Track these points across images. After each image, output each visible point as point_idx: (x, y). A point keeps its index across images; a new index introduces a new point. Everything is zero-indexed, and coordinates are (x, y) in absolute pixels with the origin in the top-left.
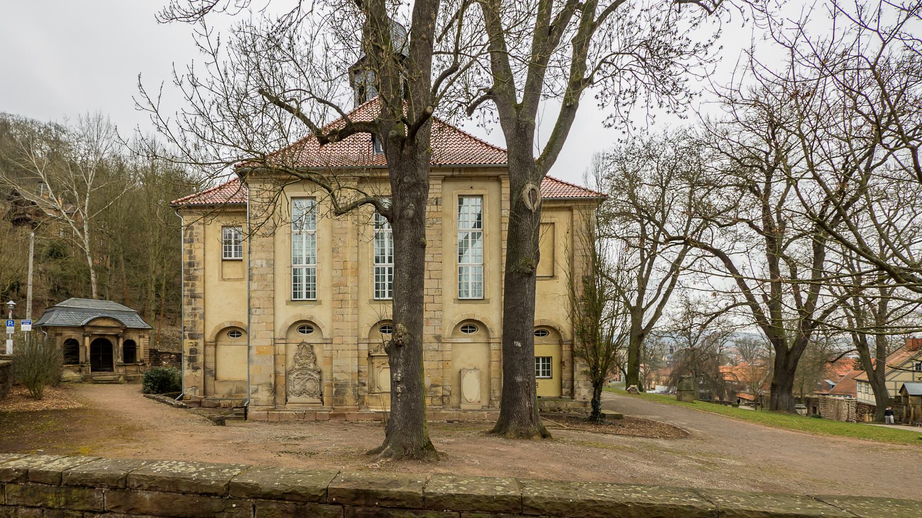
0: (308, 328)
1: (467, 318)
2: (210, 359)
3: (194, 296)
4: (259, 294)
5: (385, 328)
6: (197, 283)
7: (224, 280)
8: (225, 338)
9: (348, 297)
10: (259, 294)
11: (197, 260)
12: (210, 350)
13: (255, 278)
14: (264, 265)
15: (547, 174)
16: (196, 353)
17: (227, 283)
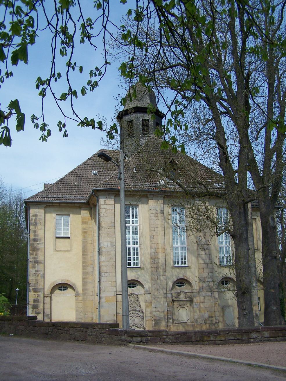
0: (133, 284)
2: (47, 306)
3: (37, 262)
4: (106, 263)
5: (61, 287)
6: (39, 253)
7: (57, 251)
8: (58, 292)
10: (106, 263)
11: (39, 237)
12: (47, 300)
13: (104, 253)
16: (38, 302)
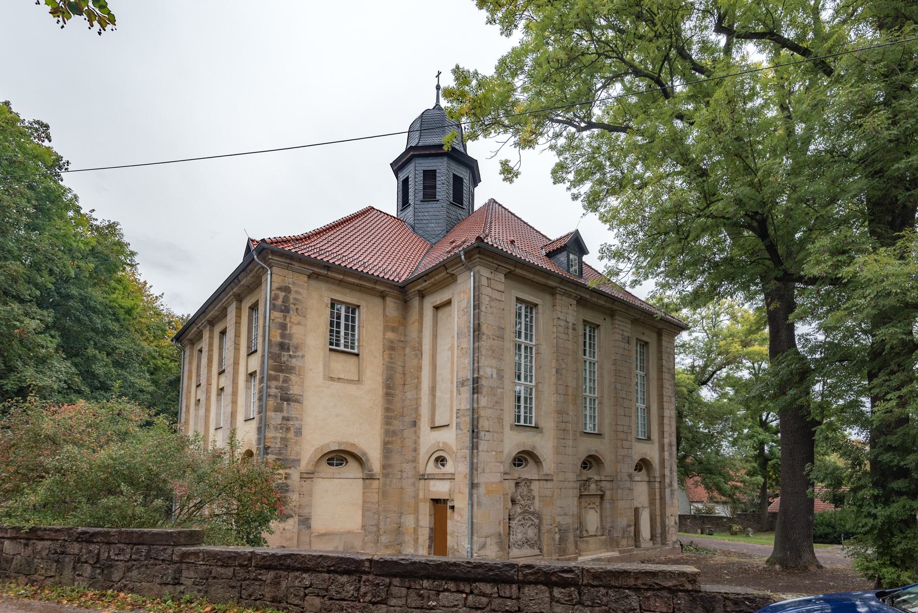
1: (342, 448)
9: (569, 426)
14: (495, 376)
15: (177, 284)
17: (337, 385)
